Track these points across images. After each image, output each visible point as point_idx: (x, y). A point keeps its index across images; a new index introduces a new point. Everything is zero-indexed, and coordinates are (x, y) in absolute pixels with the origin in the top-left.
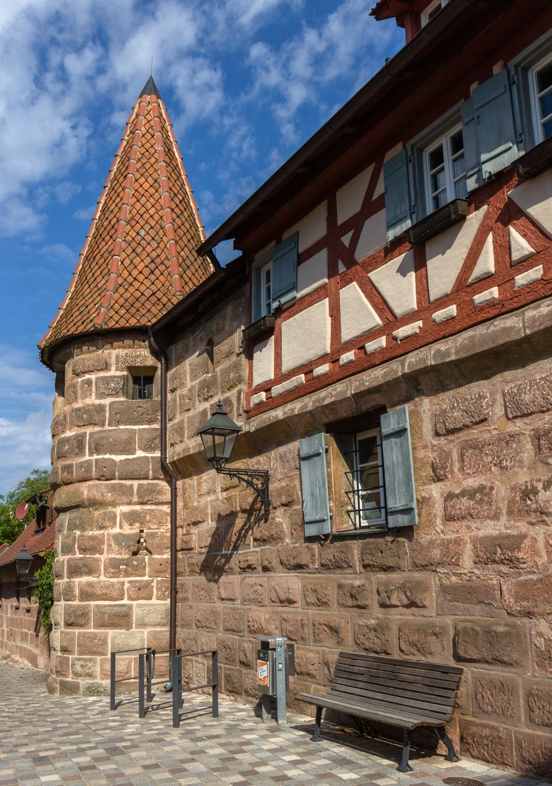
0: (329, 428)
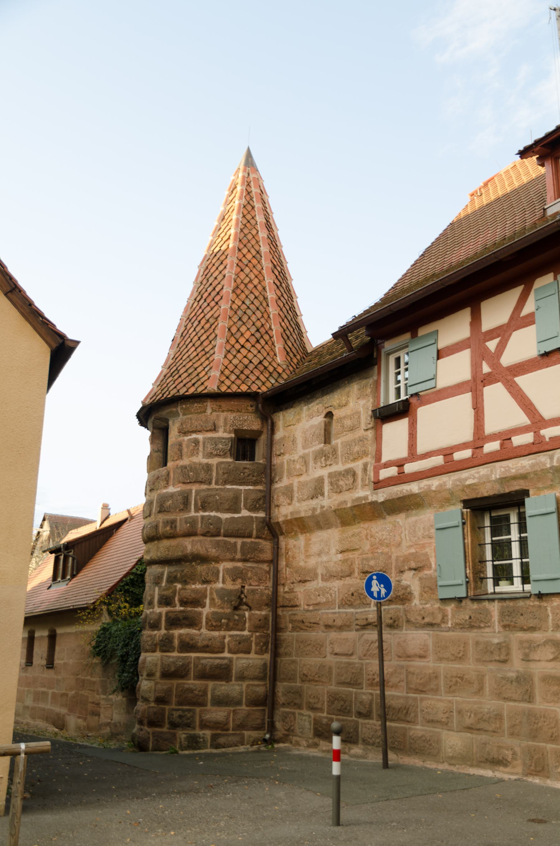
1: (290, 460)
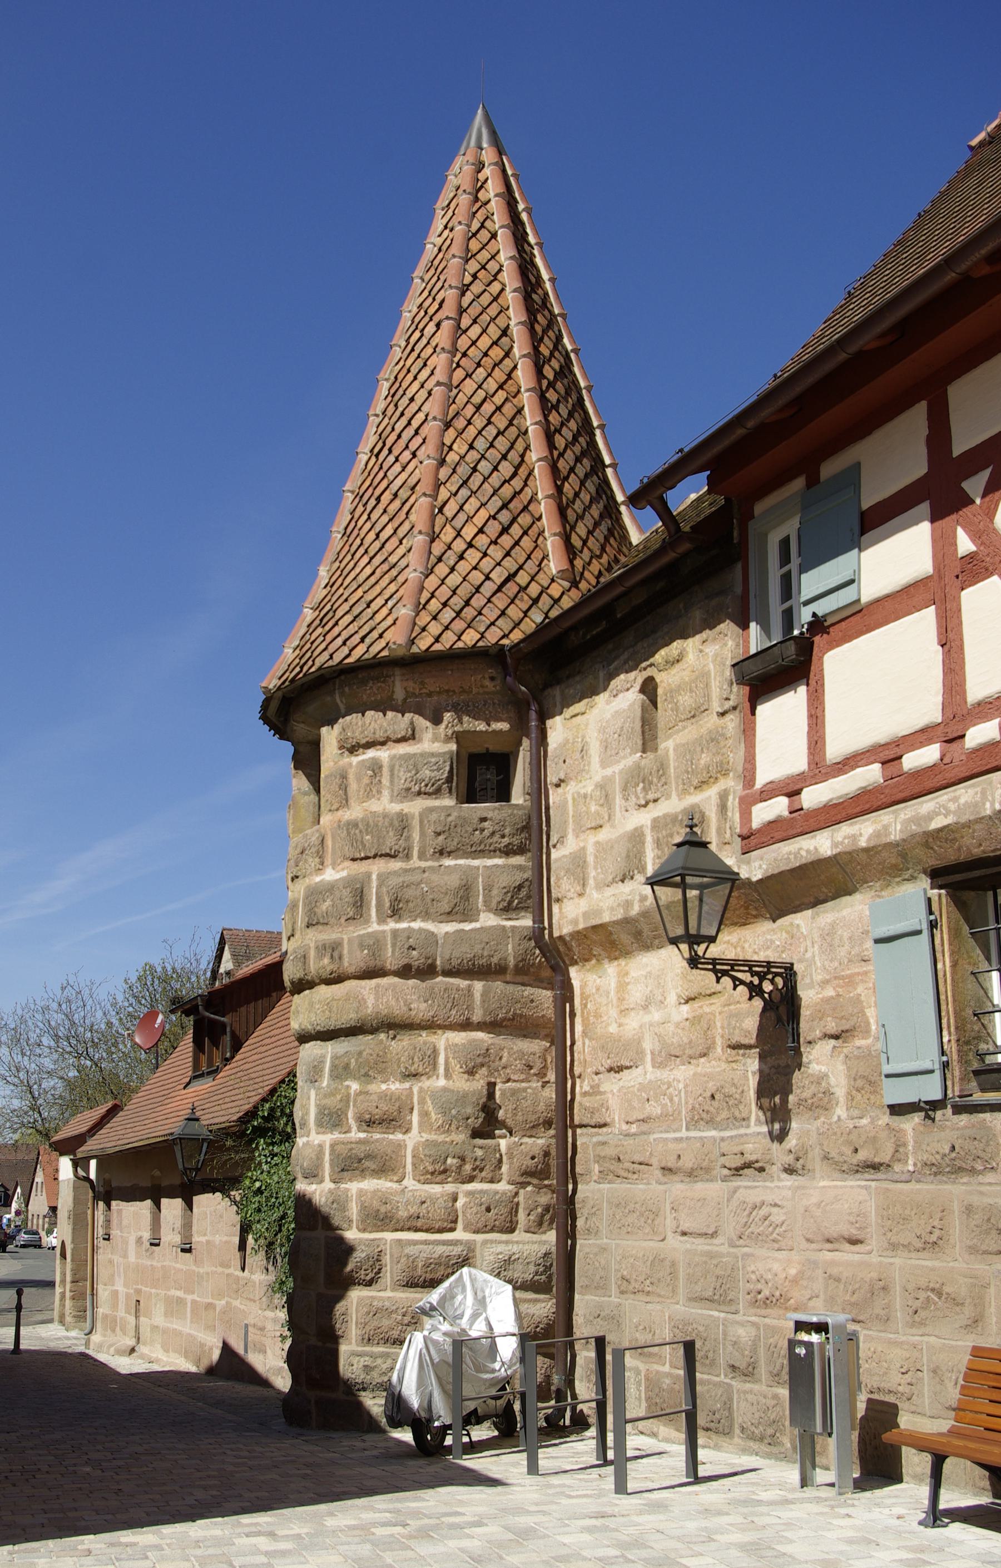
0: (937, 875)
1: (578, 793)
